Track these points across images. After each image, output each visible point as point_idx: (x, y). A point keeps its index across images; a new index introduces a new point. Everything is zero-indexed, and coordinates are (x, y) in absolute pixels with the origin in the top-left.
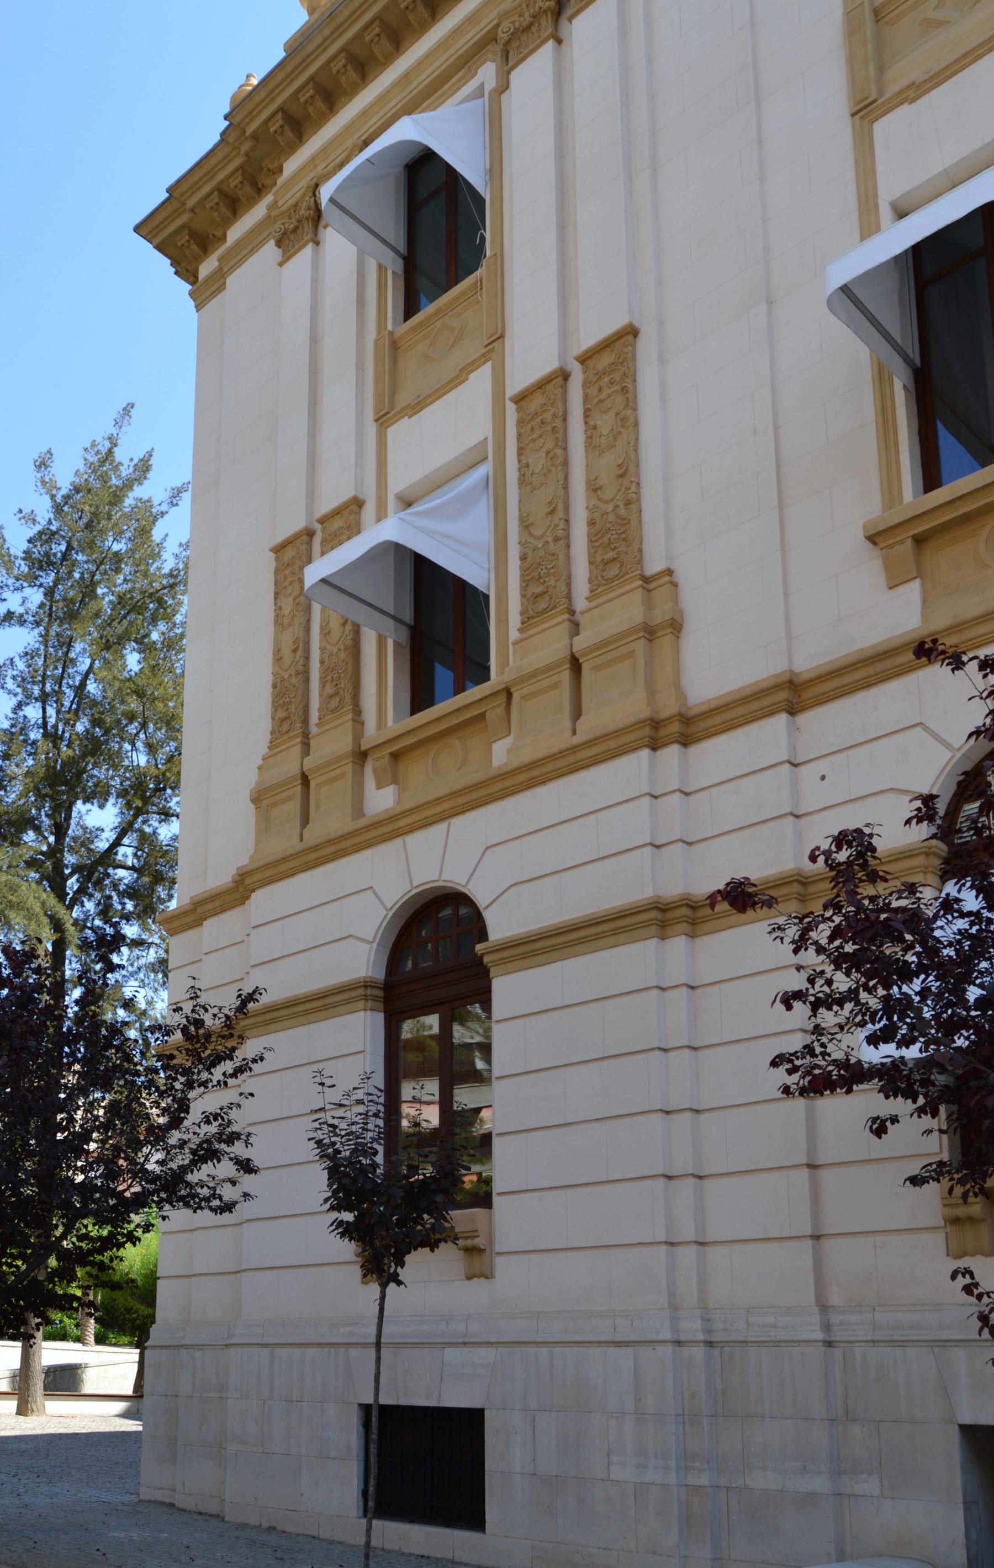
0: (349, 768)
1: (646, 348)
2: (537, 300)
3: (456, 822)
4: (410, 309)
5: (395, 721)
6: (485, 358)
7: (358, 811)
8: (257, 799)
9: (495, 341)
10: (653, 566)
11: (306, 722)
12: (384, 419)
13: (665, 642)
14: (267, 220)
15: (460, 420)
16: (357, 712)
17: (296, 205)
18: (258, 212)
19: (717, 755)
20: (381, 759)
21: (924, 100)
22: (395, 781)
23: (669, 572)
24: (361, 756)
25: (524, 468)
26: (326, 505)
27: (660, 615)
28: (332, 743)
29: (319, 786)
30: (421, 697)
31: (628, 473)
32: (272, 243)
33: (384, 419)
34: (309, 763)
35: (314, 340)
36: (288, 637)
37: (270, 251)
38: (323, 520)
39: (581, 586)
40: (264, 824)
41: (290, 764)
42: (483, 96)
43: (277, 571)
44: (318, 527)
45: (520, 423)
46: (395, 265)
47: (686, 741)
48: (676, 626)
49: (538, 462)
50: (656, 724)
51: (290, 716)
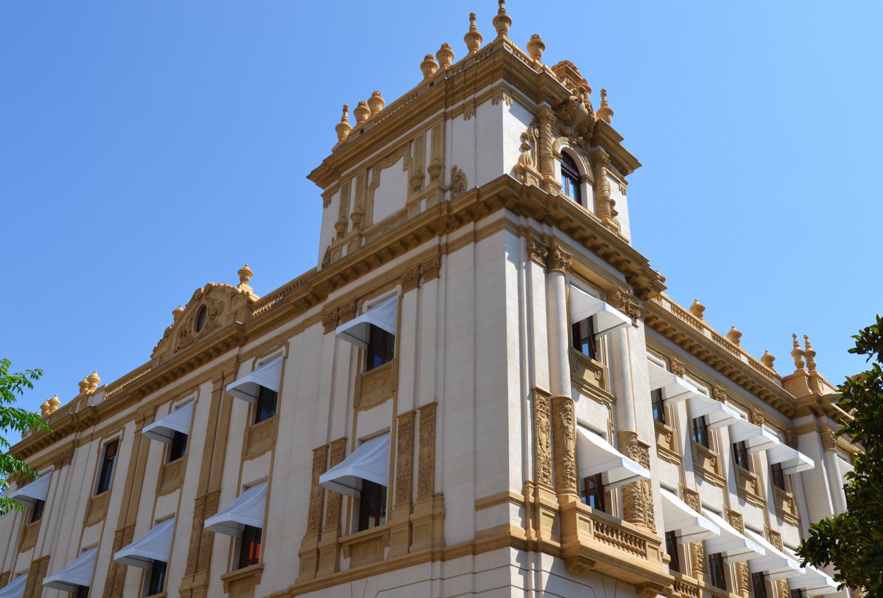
0: (335, 550)
1: (439, 408)
2: (415, 377)
3: (369, 579)
4: (257, 420)
5: (233, 570)
6: (102, 519)
7: (337, 569)
8: (300, 555)
9: (395, 390)
10: (438, 490)
11: (321, 525)
12: (358, 407)
13: (438, 522)
14: (135, 413)
15: (379, 417)
16: (340, 526)
17: (348, 304)
18: (317, 309)
19: (453, 566)
20: (346, 547)
21: (370, 411)
22: (351, 556)
23: (442, 495)
24: (339, 545)
25: (421, 436)
26: (43, 556)
27: (438, 510)
28: (329, 538)
29: (417, 527)
30: (363, 525)
31: (432, 455)
32: (133, 422)
33: (358, 407)
34: (413, 517)
35: (334, 370)
36: (195, 534)
37: (319, 327)
38: (333, 443)
39: (415, 496)
40: (303, 568)
41: (312, 545)
42: (21, 484)
43: (314, 460)
44: (418, 412)
45: (421, 418)
46: (364, 347)
47: (443, 560)
48: (443, 516)
49: (426, 435)
50: (433, 553)
51: (315, 524)
